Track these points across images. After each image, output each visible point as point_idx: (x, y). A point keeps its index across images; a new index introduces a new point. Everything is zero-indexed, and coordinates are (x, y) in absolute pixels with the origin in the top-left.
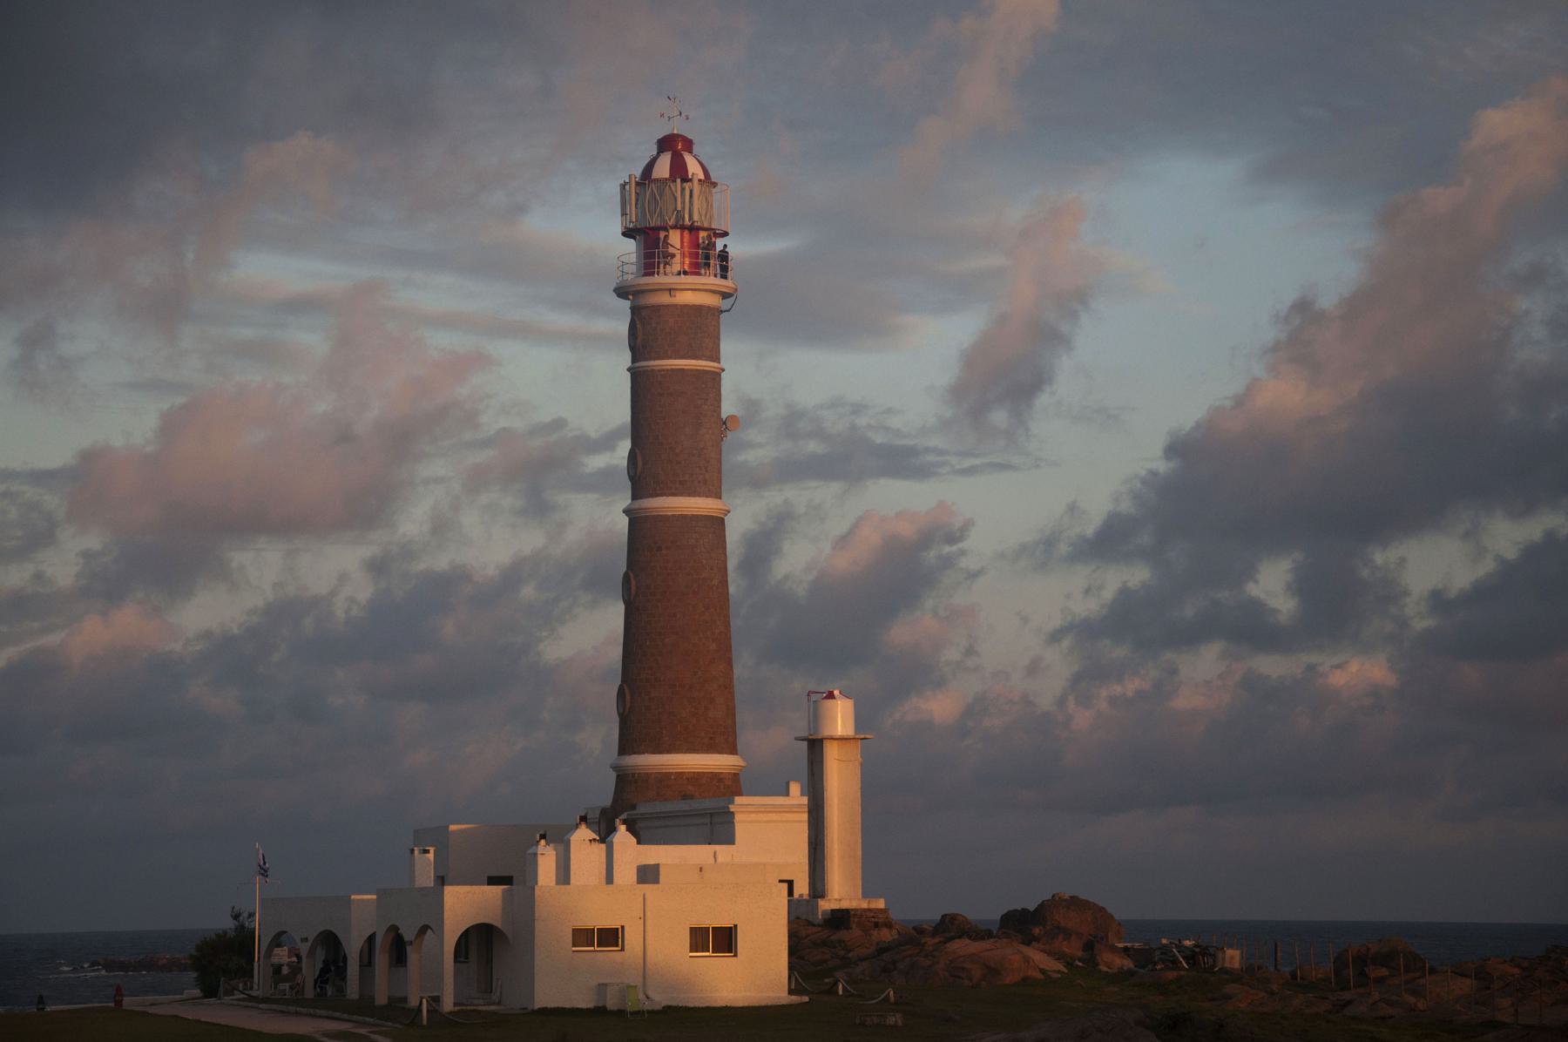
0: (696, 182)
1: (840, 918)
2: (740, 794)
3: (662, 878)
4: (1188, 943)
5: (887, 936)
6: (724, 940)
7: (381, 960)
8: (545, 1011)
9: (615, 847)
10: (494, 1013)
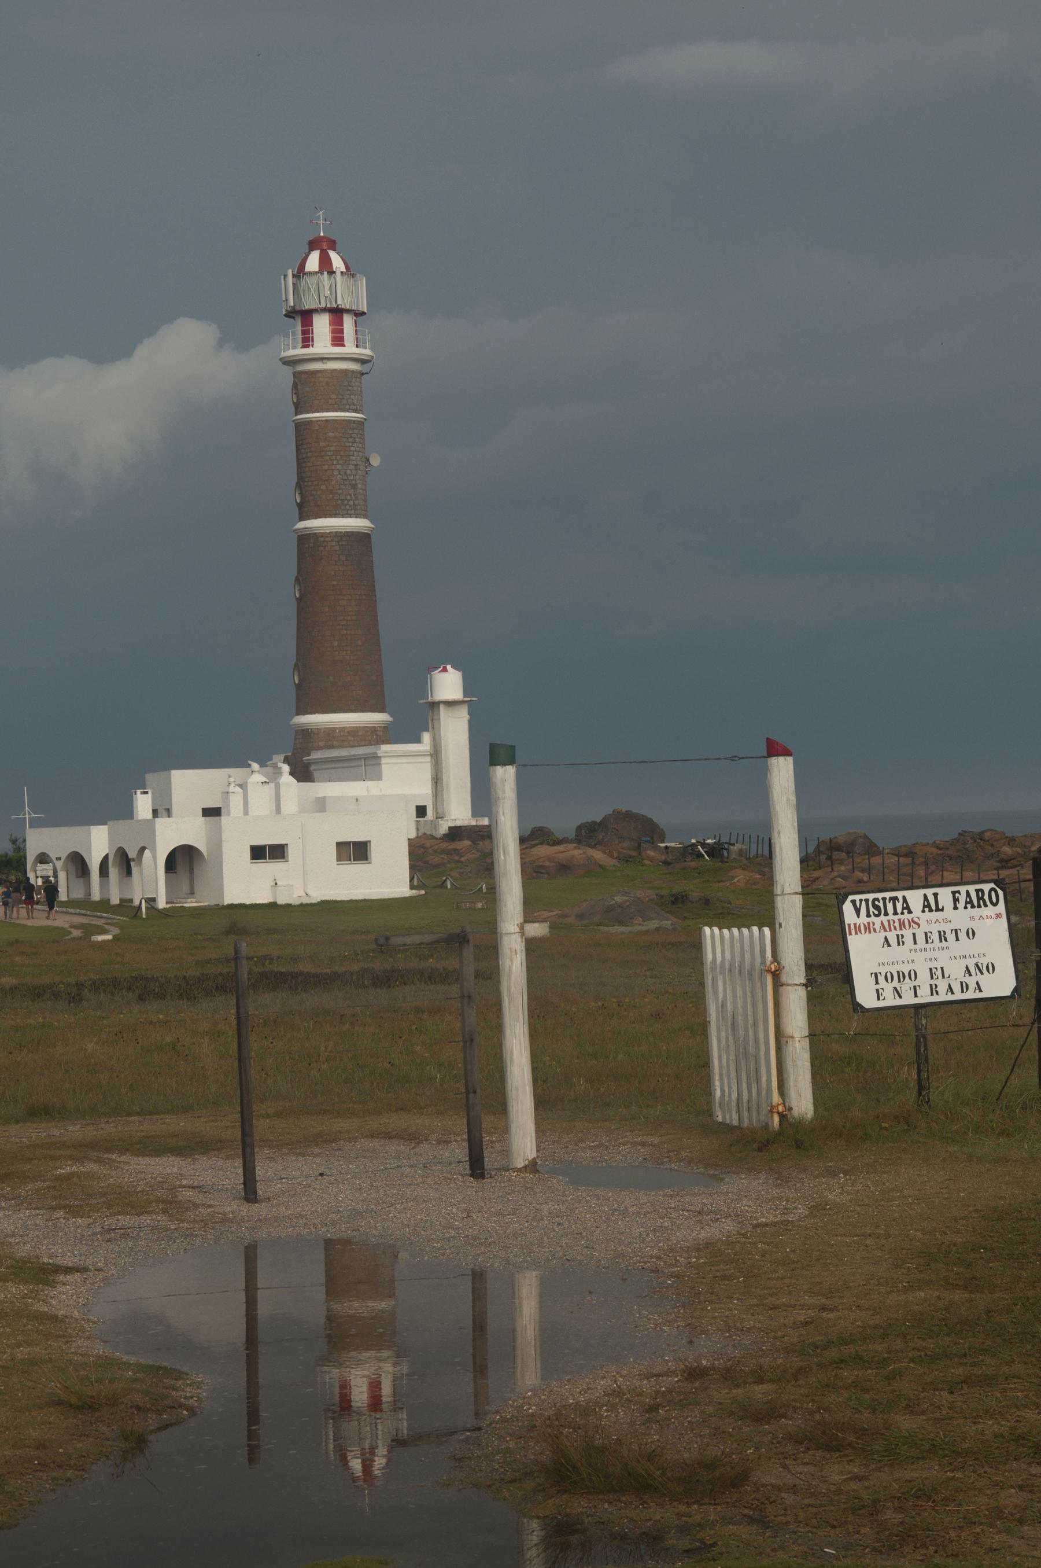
0: (338, 274)
1: (455, 833)
4: (709, 841)
6: (356, 851)
7: (113, 872)
8: (231, 906)
10: (195, 908)
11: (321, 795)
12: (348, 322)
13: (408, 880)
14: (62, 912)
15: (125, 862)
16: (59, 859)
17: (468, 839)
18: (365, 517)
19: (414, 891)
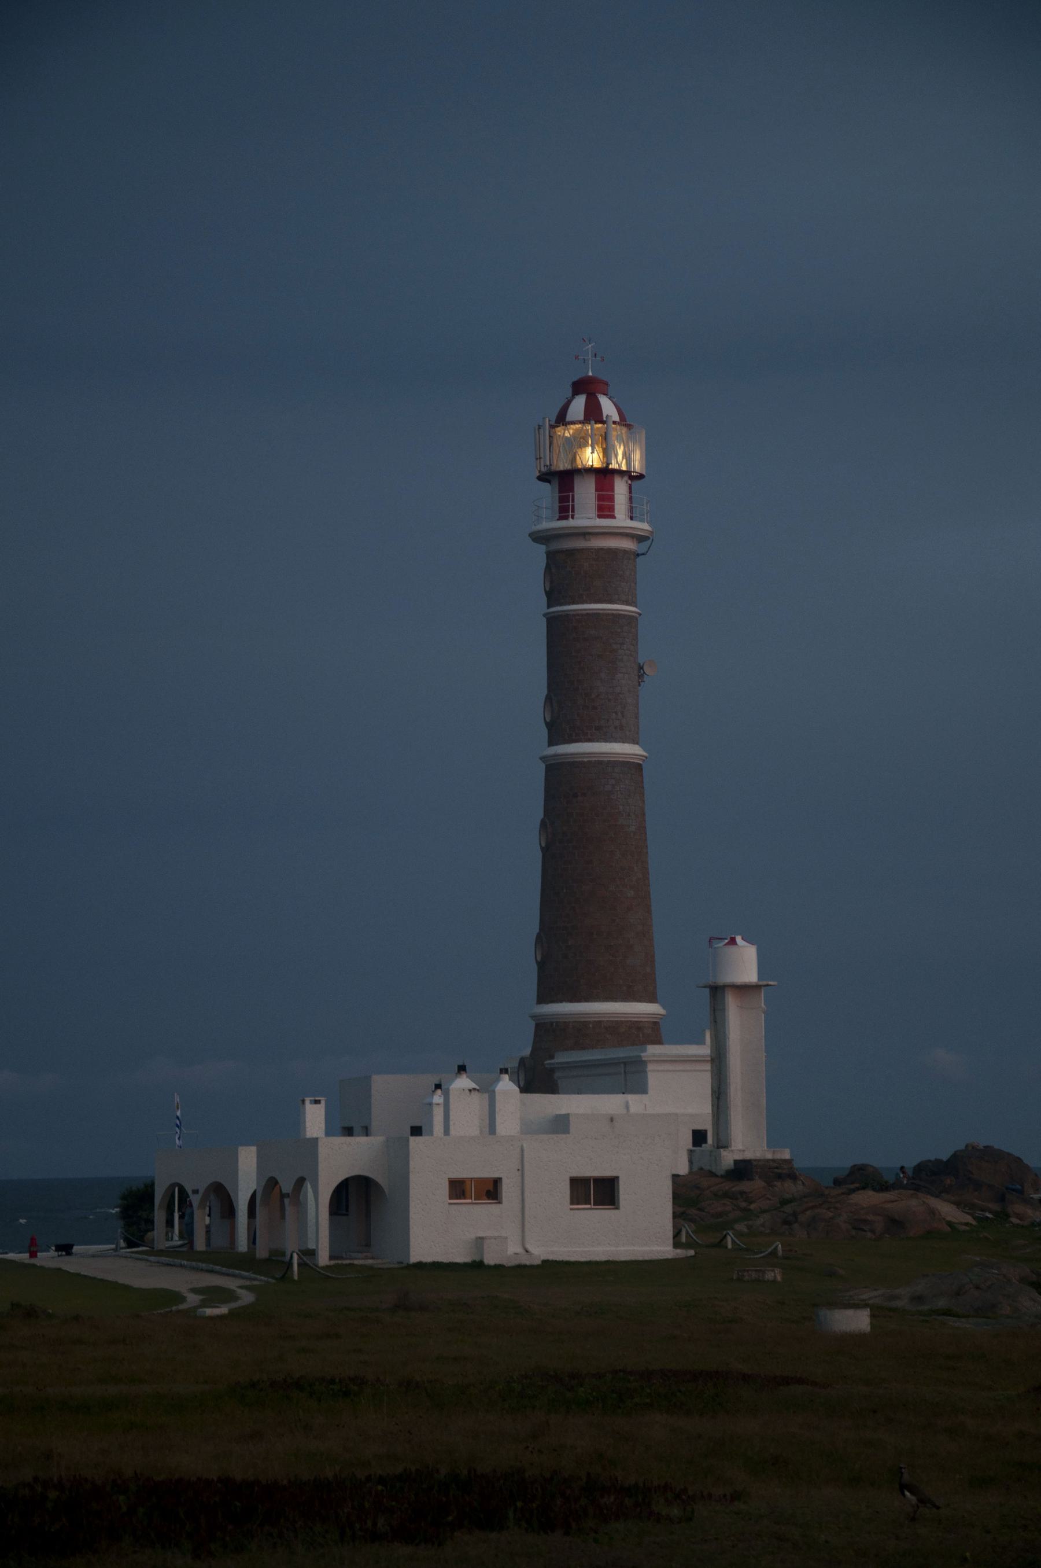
1: (743, 1170)
2: (659, 1042)
3: (572, 1130)
5: (790, 1188)
6: (598, 1192)
8: (420, 1265)
9: (498, 1097)
10: (371, 1268)
11: (563, 1112)
12: (620, 488)
13: (670, 1234)
14: (193, 1269)
15: (278, 1196)
16: (195, 1192)
18: (635, 742)
19: (679, 1251)
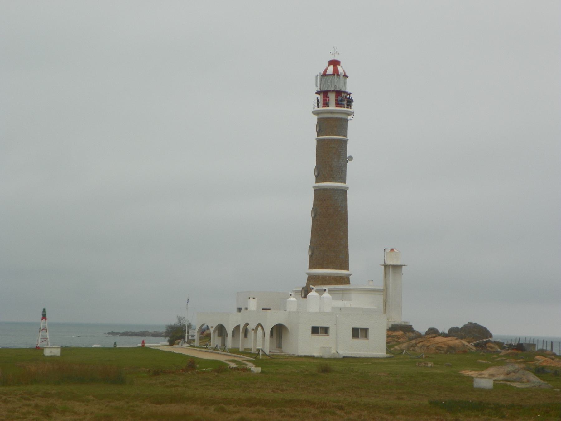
6: (358, 333)
14: (216, 353)
17: (402, 331)
